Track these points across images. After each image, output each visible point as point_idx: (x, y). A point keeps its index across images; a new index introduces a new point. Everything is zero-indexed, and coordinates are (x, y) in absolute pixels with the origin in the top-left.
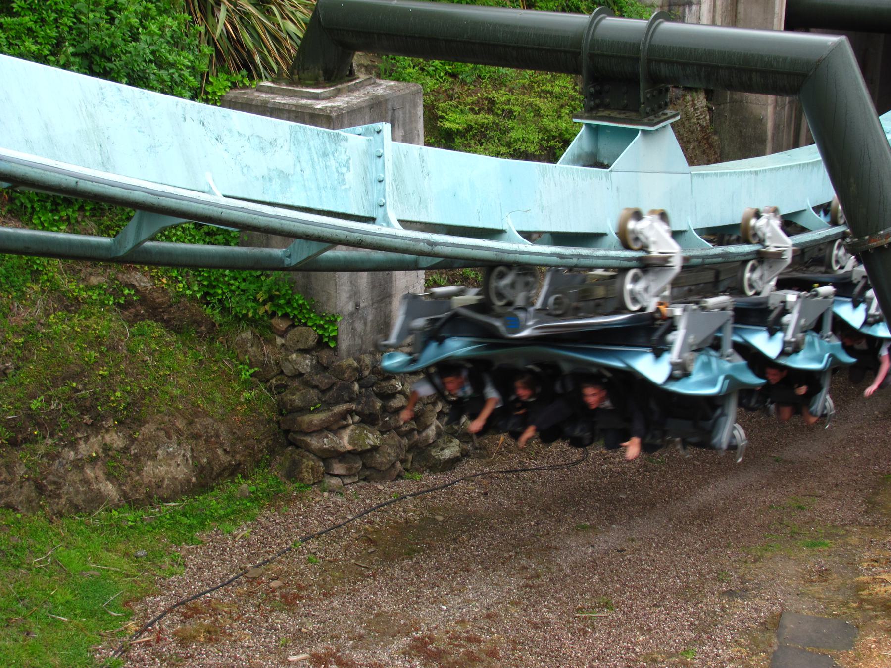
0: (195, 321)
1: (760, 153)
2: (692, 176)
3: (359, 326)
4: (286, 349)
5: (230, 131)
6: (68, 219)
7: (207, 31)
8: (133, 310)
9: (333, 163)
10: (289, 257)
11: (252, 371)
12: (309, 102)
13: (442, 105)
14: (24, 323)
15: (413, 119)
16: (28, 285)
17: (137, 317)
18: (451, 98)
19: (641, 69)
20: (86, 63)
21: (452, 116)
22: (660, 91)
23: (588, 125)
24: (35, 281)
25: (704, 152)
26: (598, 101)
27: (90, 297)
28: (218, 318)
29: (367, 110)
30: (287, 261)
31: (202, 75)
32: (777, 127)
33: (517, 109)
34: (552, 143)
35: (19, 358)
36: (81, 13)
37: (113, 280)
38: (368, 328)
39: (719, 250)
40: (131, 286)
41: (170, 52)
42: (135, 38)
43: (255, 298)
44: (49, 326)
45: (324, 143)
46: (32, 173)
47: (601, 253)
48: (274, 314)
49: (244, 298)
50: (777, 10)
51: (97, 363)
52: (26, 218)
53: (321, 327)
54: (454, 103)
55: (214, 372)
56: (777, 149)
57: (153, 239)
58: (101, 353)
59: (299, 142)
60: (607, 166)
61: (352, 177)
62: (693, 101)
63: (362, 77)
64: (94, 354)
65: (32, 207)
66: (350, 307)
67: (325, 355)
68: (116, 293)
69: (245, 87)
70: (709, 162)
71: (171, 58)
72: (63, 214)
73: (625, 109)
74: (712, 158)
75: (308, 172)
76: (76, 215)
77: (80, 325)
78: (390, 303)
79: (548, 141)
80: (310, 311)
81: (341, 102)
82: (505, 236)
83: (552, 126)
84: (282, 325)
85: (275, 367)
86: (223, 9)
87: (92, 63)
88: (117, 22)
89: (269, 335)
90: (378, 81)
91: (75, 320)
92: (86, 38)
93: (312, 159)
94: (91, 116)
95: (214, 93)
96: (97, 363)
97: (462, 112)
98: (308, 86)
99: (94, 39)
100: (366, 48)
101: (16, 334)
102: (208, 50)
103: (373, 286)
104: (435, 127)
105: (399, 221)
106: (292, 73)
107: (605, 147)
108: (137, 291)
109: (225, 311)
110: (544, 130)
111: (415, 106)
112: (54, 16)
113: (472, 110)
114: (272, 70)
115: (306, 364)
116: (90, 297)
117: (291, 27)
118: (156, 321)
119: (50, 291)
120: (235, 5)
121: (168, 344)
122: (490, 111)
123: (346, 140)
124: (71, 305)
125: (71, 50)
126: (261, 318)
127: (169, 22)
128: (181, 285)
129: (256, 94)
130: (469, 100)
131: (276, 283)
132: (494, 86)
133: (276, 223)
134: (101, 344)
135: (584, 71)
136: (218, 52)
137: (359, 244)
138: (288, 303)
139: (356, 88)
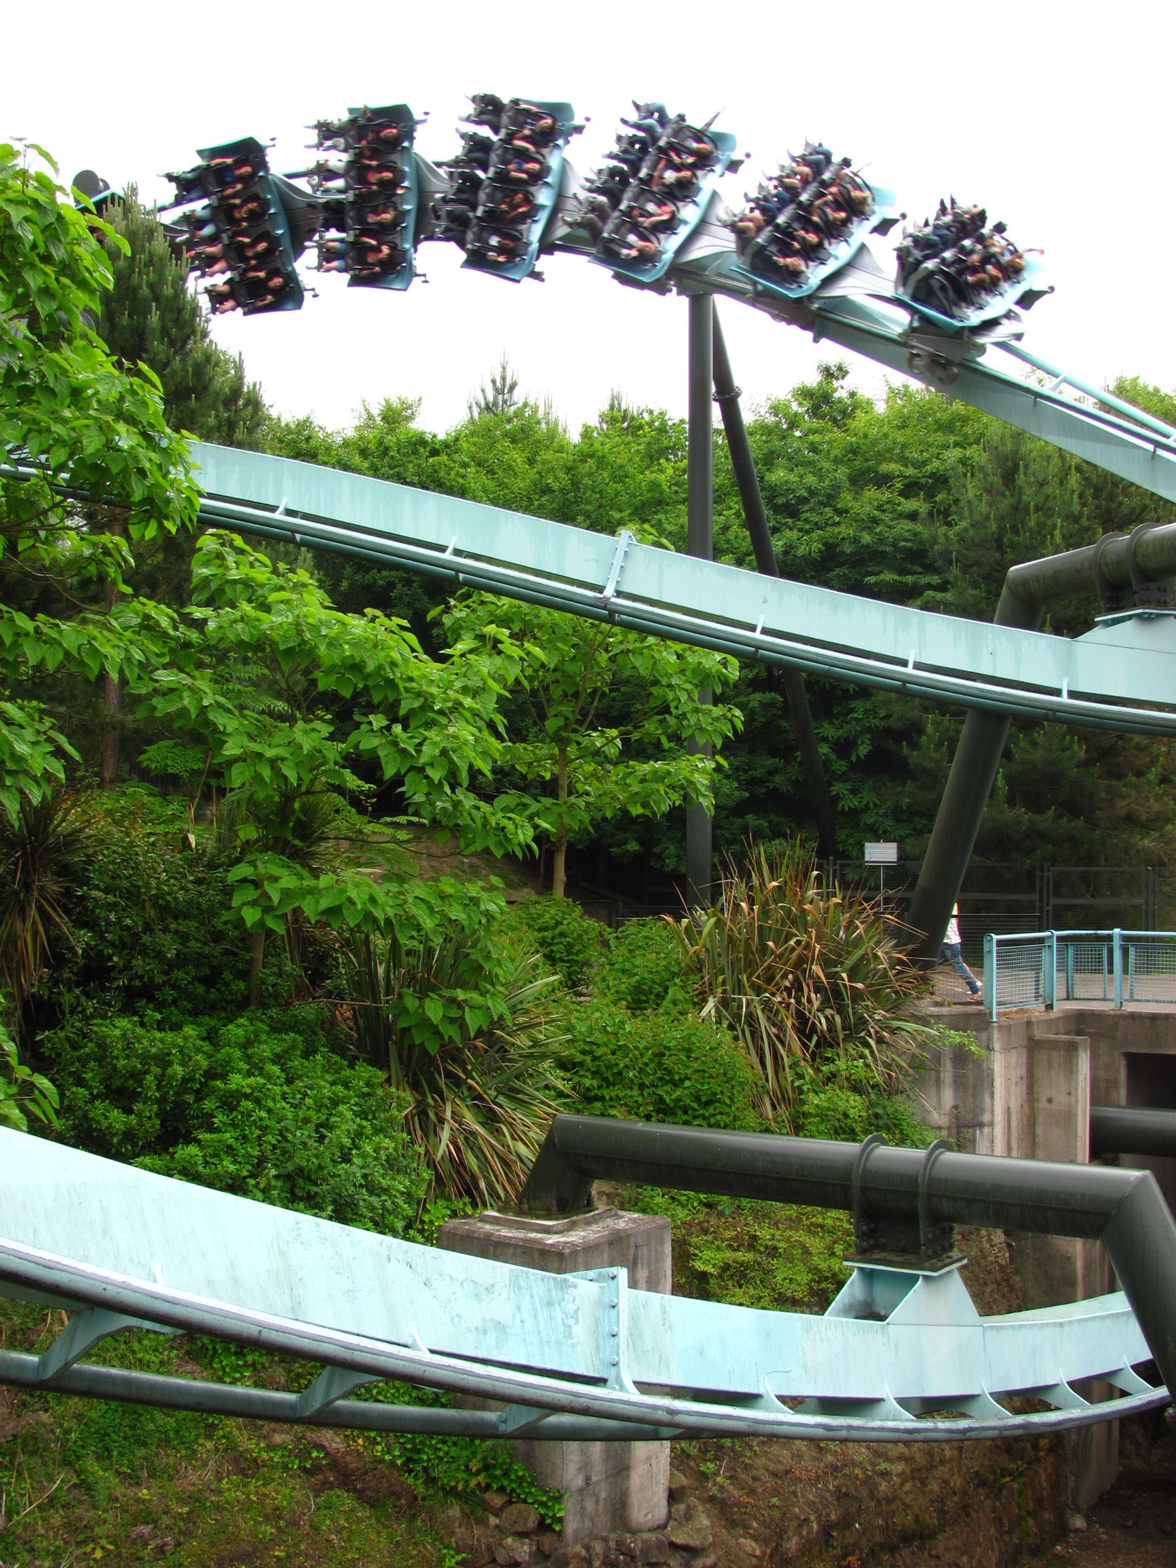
0: (393, 1493)
1: (1069, 1299)
2: (985, 1329)
3: (590, 1505)
4: (501, 1531)
5: (441, 1274)
6: (254, 1364)
7: (427, 1152)
8: (320, 1477)
9: (558, 1314)
10: (505, 1422)
11: (459, 1558)
12: (540, 1235)
13: (694, 1240)
14: (191, 1489)
15: (658, 1258)
16: (201, 1441)
17: (325, 1485)
18: (705, 1232)
19: (921, 1205)
20: (289, 1185)
21: (707, 1254)
22: (943, 1231)
23: (860, 1269)
24: (209, 1437)
25: (1004, 1296)
26: (872, 1242)
27: (271, 1459)
28: (421, 1490)
29: (606, 1247)
30: (502, 1428)
31: (418, 1203)
32: (1088, 1267)
33: (782, 1245)
34: (823, 1285)
35: (181, 1532)
36: (287, 1130)
37: (300, 1439)
38: (601, 1508)
39: (1020, 1419)
40: (320, 1447)
41: (383, 1176)
42: (346, 1159)
43: (467, 1467)
44: (220, 1492)
45: (549, 1290)
46: (210, 1320)
47: (876, 1424)
48: (488, 1487)
49: (454, 1466)
50: (1080, 1132)
51: (273, 1542)
52: (206, 1361)
53: (544, 1504)
54: (709, 1238)
55: (412, 1557)
56: (1090, 1294)
57: (345, 1396)
58: (279, 1529)
59: (520, 1288)
60: (881, 1318)
61: (580, 1331)
62: (989, 1236)
63: (601, 1207)
64: (270, 1529)
65: (214, 1349)
66: (579, 1481)
67: (547, 1541)
68: (303, 1455)
69: (466, 1216)
70: (1010, 1311)
71: (385, 1183)
72: (250, 1358)
73: (904, 1250)
74: (1014, 1303)
75: (530, 1323)
76: (263, 1360)
77: (257, 1493)
78: (628, 1477)
79: (819, 1283)
80: (531, 1484)
81: (576, 1237)
82: (762, 1402)
83: (823, 1266)
84: (497, 1501)
85: (486, 1554)
86: (446, 1127)
87: (294, 1185)
88: (326, 1141)
89: (480, 1513)
90: (621, 1213)
91: (252, 1487)
92: (291, 1158)
93: (535, 1309)
94: (282, 1254)
95: (431, 1222)
96: (273, 1542)
97: (718, 1248)
98: (538, 1217)
99: (300, 1159)
100: (607, 1175)
101: (181, 1501)
102: (427, 1174)
103: (608, 1456)
104: (686, 1267)
105: (635, 1383)
106: (521, 1202)
107: (881, 1293)
108: (327, 1454)
109: (431, 1481)
110: (815, 1270)
111: (662, 1242)
112: (258, 1132)
113: (730, 1246)
114: (499, 1197)
115: (523, 1550)
116: (271, 1459)
117: (522, 1149)
118: (348, 1491)
119: (225, 1450)
120: (461, 1124)
121: (360, 1521)
122: (751, 1247)
123: (575, 1286)
124: (248, 1467)
125: (273, 1172)
126: (473, 1492)
127: (387, 1143)
128: (379, 1448)
129: (479, 1224)
130: (729, 1234)
131: (493, 1449)
132: (756, 1218)
133: (487, 1385)
134: (279, 1517)
135: (855, 1206)
136: (438, 1176)
137: (585, 1411)
138: (506, 1474)
139: (594, 1220)
